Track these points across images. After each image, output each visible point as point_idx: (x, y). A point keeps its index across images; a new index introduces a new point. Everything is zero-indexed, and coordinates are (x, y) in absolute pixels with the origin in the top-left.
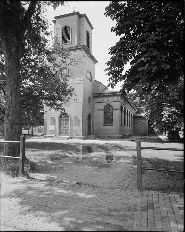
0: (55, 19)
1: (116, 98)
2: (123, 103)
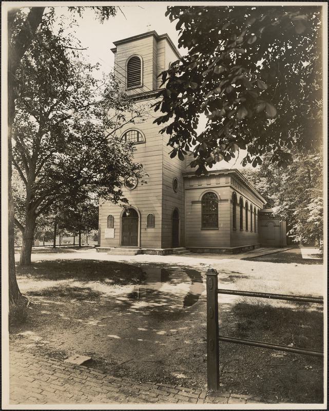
0: (114, 47)
1: (223, 181)
2: (237, 190)
